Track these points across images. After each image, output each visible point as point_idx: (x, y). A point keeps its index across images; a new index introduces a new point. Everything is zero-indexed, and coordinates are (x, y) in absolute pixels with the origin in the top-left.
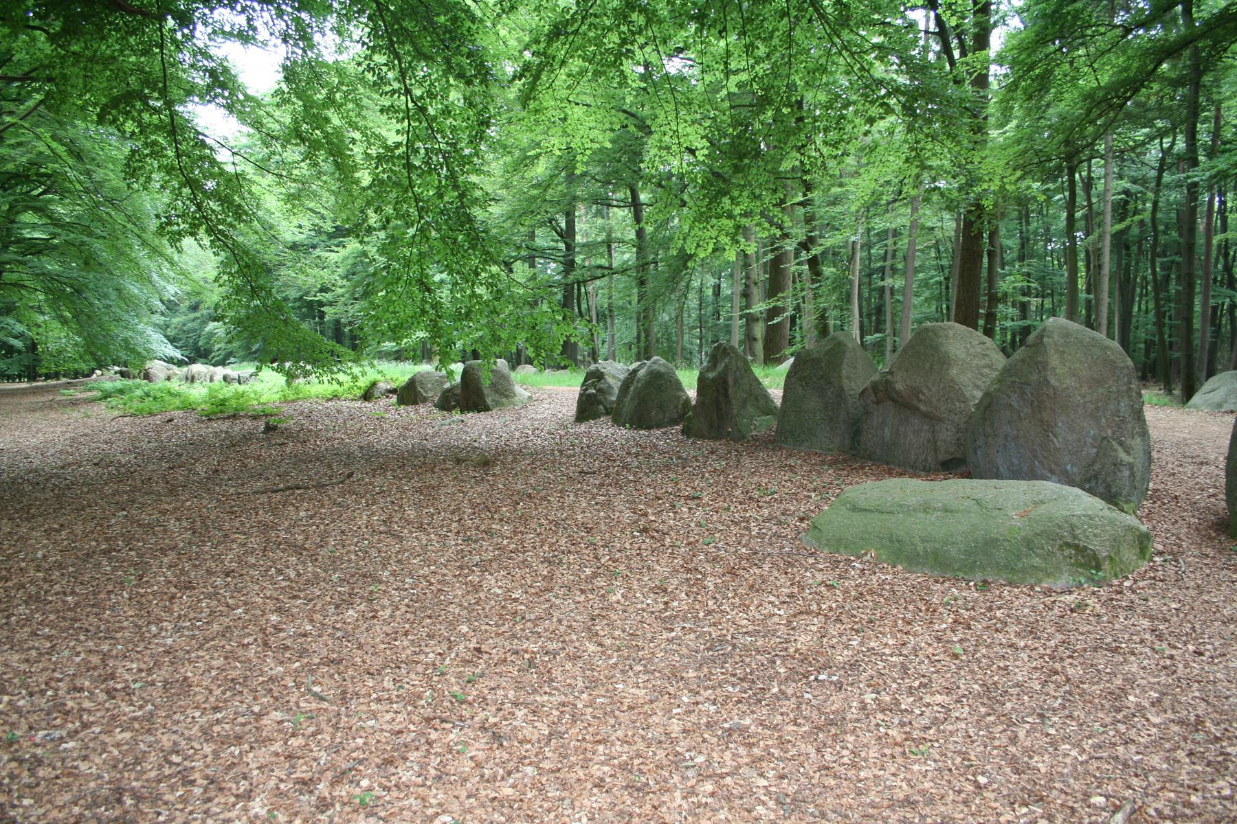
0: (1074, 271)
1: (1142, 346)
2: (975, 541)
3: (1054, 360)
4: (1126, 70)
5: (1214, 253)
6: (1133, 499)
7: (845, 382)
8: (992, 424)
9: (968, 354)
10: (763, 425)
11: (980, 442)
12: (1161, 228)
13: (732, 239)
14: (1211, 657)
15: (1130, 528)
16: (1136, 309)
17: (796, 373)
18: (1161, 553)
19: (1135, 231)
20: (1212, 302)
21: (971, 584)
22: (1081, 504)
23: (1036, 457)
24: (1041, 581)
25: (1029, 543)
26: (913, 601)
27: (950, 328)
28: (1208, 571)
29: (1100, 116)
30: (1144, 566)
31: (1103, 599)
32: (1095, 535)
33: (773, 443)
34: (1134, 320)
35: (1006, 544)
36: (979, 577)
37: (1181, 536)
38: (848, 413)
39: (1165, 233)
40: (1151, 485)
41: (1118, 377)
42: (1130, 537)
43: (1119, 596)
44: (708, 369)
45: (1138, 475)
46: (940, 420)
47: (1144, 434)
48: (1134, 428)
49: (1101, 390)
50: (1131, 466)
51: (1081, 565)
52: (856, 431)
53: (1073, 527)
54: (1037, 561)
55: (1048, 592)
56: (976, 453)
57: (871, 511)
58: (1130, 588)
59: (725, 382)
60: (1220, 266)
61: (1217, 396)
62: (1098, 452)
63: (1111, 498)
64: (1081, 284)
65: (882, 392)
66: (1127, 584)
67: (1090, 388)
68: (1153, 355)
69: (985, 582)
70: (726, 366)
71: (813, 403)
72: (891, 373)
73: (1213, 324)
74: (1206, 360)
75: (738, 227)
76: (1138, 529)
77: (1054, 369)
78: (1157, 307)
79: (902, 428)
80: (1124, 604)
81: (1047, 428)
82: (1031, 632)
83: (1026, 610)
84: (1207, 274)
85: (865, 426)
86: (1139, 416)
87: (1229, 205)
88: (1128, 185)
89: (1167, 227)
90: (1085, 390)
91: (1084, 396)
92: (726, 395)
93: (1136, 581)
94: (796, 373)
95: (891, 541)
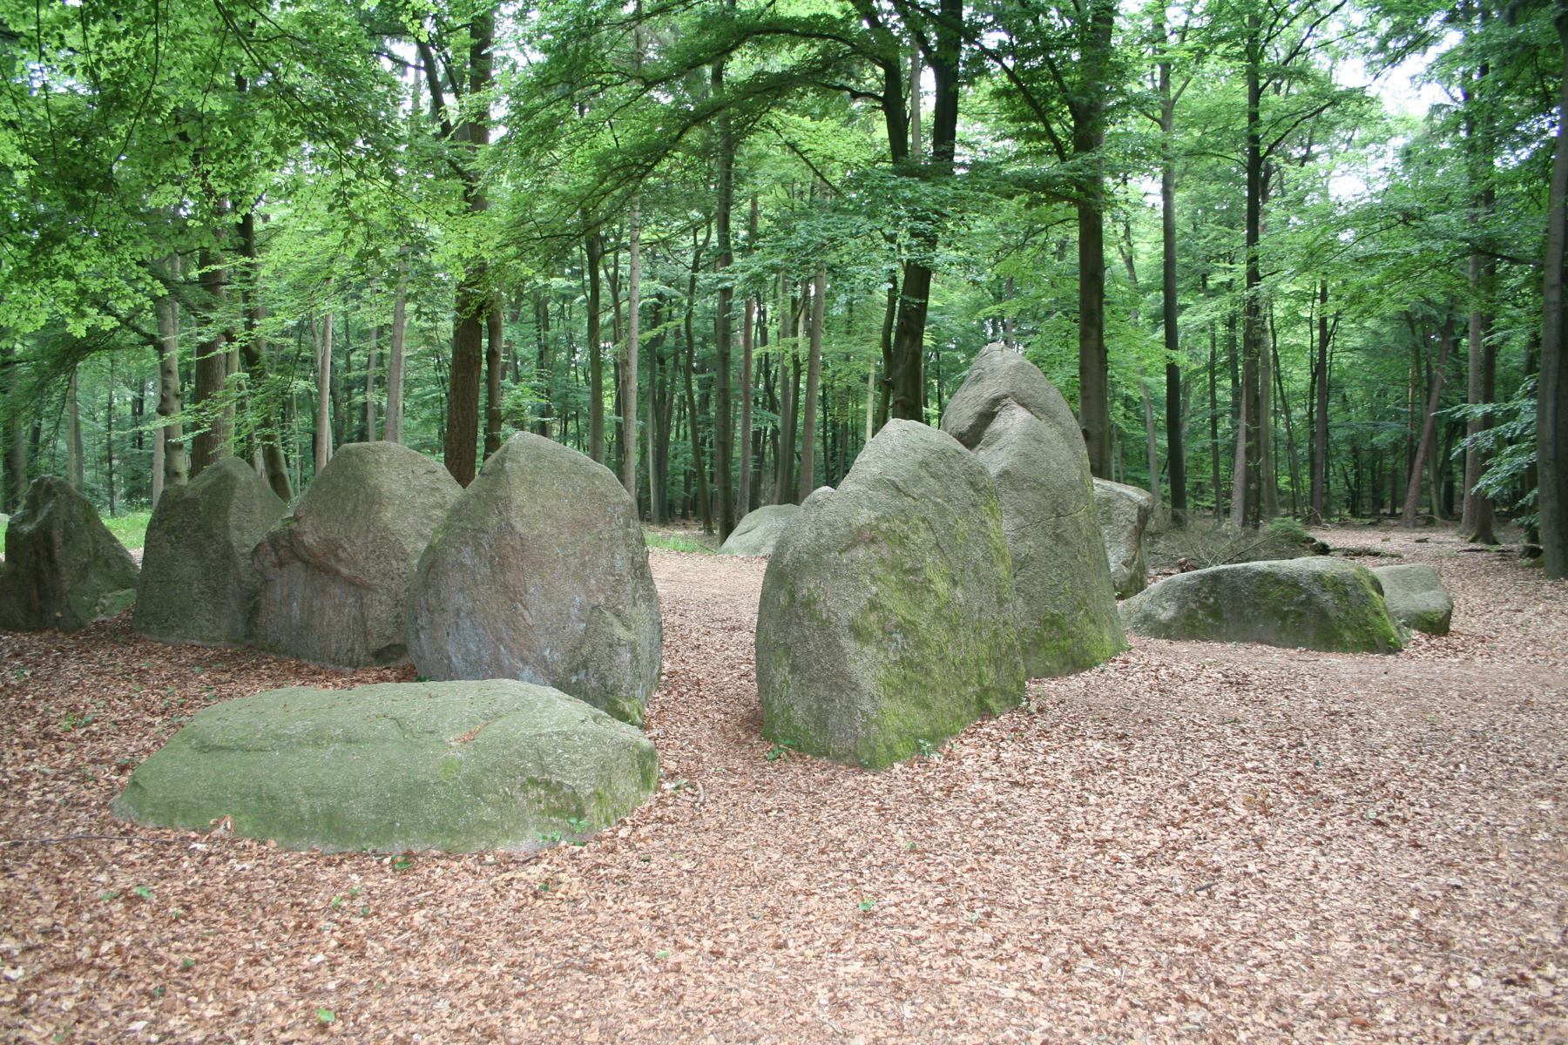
0: (597, 389)
1: (682, 478)
2: (392, 789)
3: (520, 495)
4: (647, 133)
5: (754, 368)
6: (638, 692)
7: (235, 536)
8: (438, 593)
9: (409, 487)
10: (114, 604)
11: (422, 621)
12: (698, 339)
13: (76, 309)
14: (735, 958)
15: (626, 746)
16: (673, 435)
17: (161, 522)
18: (672, 776)
19: (670, 342)
20: (753, 427)
21: (387, 861)
22: (561, 712)
23: (500, 639)
24: (494, 844)
25: (474, 785)
26: (278, 910)
27: (383, 450)
28: (735, 797)
29: (617, 186)
30: (650, 799)
31: (587, 865)
32: (574, 763)
33: (126, 633)
34: (671, 449)
35: (440, 789)
36: (399, 847)
37: (702, 743)
38: (240, 582)
39: (703, 345)
40: (667, 665)
41: (611, 518)
42: (626, 760)
43: (609, 859)
44: (24, 520)
45: (644, 657)
46: (369, 588)
47: (651, 597)
48: (635, 590)
49: (587, 538)
50: (633, 647)
51: (556, 812)
52: (252, 605)
53: (540, 753)
54: (488, 813)
55: (503, 864)
56: (418, 637)
57: (231, 750)
58: (626, 840)
59: (49, 539)
60: (761, 386)
61: (753, 538)
62: (587, 629)
63: (606, 699)
64: (609, 403)
65: (285, 547)
66: (623, 833)
67: (572, 534)
68: (693, 489)
69: (408, 855)
70: (50, 514)
71: (187, 568)
72: (296, 519)
73: (756, 451)
74: (748, 494)
75: (82, 292)
76: (637, 745)
77: (521, 507)
78: (695, 432)
79: (316, 603)
80: (616, 872)
81: (514, 596)
82: (463, 951)
83: (465, 904)
84: (746, 392)
85: (263, 601)
86: (641, 571)
87: (768, 316)
88: (663, 288)
89: (705, 339)
90: (565, 537)
91: (564, 548)
92: (51, 559)
93: (635, 827)
94: (161, 522)
95: (260, 799)
